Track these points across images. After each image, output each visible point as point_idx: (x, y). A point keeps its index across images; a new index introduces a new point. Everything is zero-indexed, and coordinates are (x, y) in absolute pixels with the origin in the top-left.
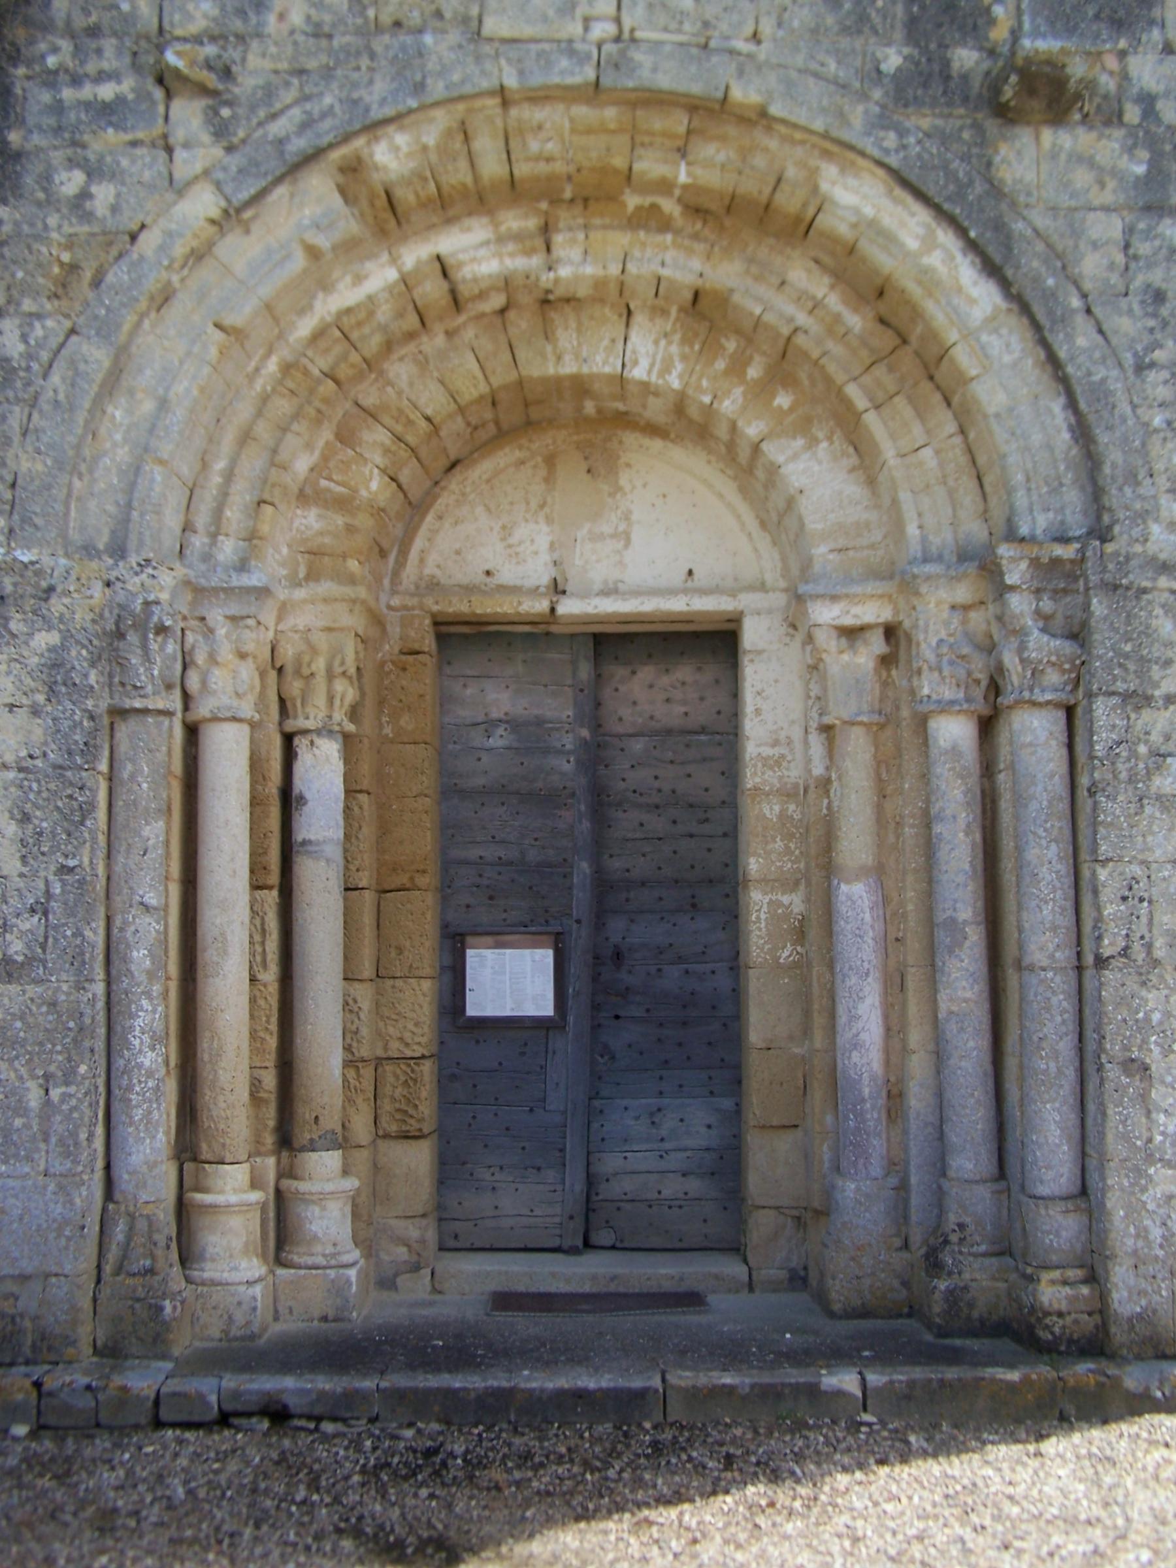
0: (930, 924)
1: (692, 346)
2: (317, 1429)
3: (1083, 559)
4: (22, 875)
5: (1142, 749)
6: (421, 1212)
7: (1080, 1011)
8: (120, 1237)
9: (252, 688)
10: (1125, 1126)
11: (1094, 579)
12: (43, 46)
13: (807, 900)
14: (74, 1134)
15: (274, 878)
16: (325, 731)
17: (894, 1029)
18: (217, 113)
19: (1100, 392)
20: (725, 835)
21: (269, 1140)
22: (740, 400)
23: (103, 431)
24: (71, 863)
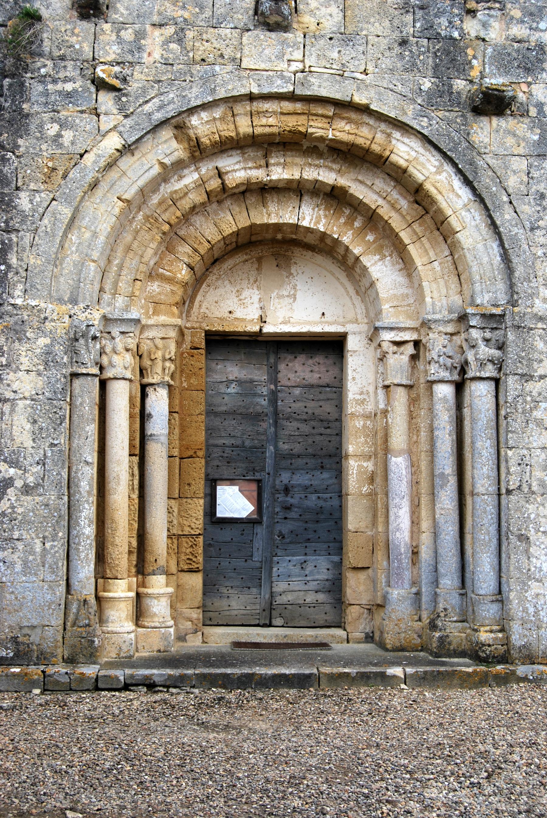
0: (432, 475)
1: (329, 211)
2: (168, 691)
3: (504, 315)
4: (33, 447)
5: (529, 399)
6: (197, 606)
7: (499, 514)
8: (74, 610)
9: (131, 364)
10: (518, 564)
11: (509, 324)
12: (39, 64)
13: (376, 465)
14: (56, 563)
15: (137, 452)
16: (161, 384)
17: (415, 522)
18: (120, 99)
19: (515, 239)
20: (337, 434)
21: (134, 570)
22: (351, 237)
23: (66, 245)
24: (56, 442)
